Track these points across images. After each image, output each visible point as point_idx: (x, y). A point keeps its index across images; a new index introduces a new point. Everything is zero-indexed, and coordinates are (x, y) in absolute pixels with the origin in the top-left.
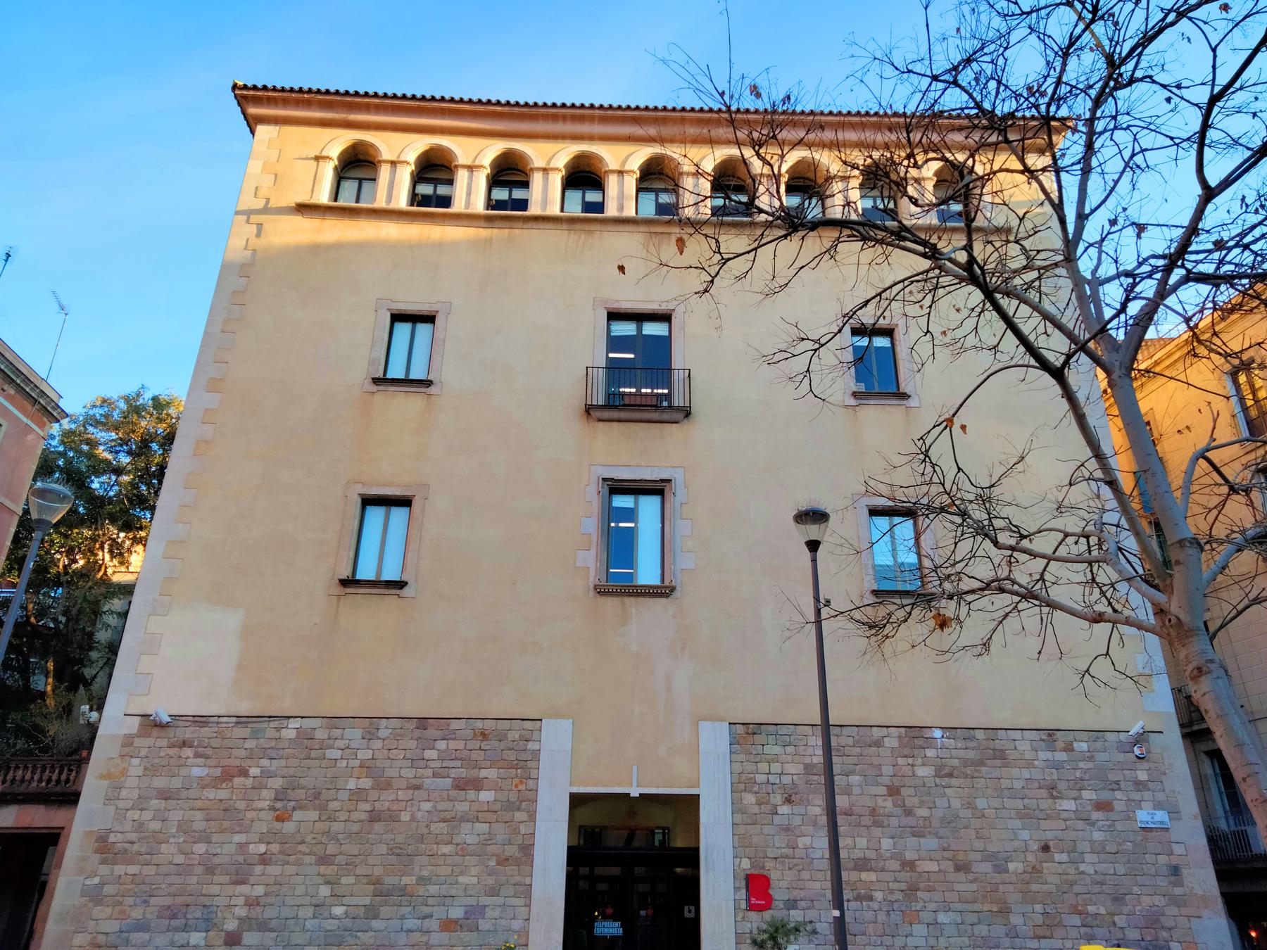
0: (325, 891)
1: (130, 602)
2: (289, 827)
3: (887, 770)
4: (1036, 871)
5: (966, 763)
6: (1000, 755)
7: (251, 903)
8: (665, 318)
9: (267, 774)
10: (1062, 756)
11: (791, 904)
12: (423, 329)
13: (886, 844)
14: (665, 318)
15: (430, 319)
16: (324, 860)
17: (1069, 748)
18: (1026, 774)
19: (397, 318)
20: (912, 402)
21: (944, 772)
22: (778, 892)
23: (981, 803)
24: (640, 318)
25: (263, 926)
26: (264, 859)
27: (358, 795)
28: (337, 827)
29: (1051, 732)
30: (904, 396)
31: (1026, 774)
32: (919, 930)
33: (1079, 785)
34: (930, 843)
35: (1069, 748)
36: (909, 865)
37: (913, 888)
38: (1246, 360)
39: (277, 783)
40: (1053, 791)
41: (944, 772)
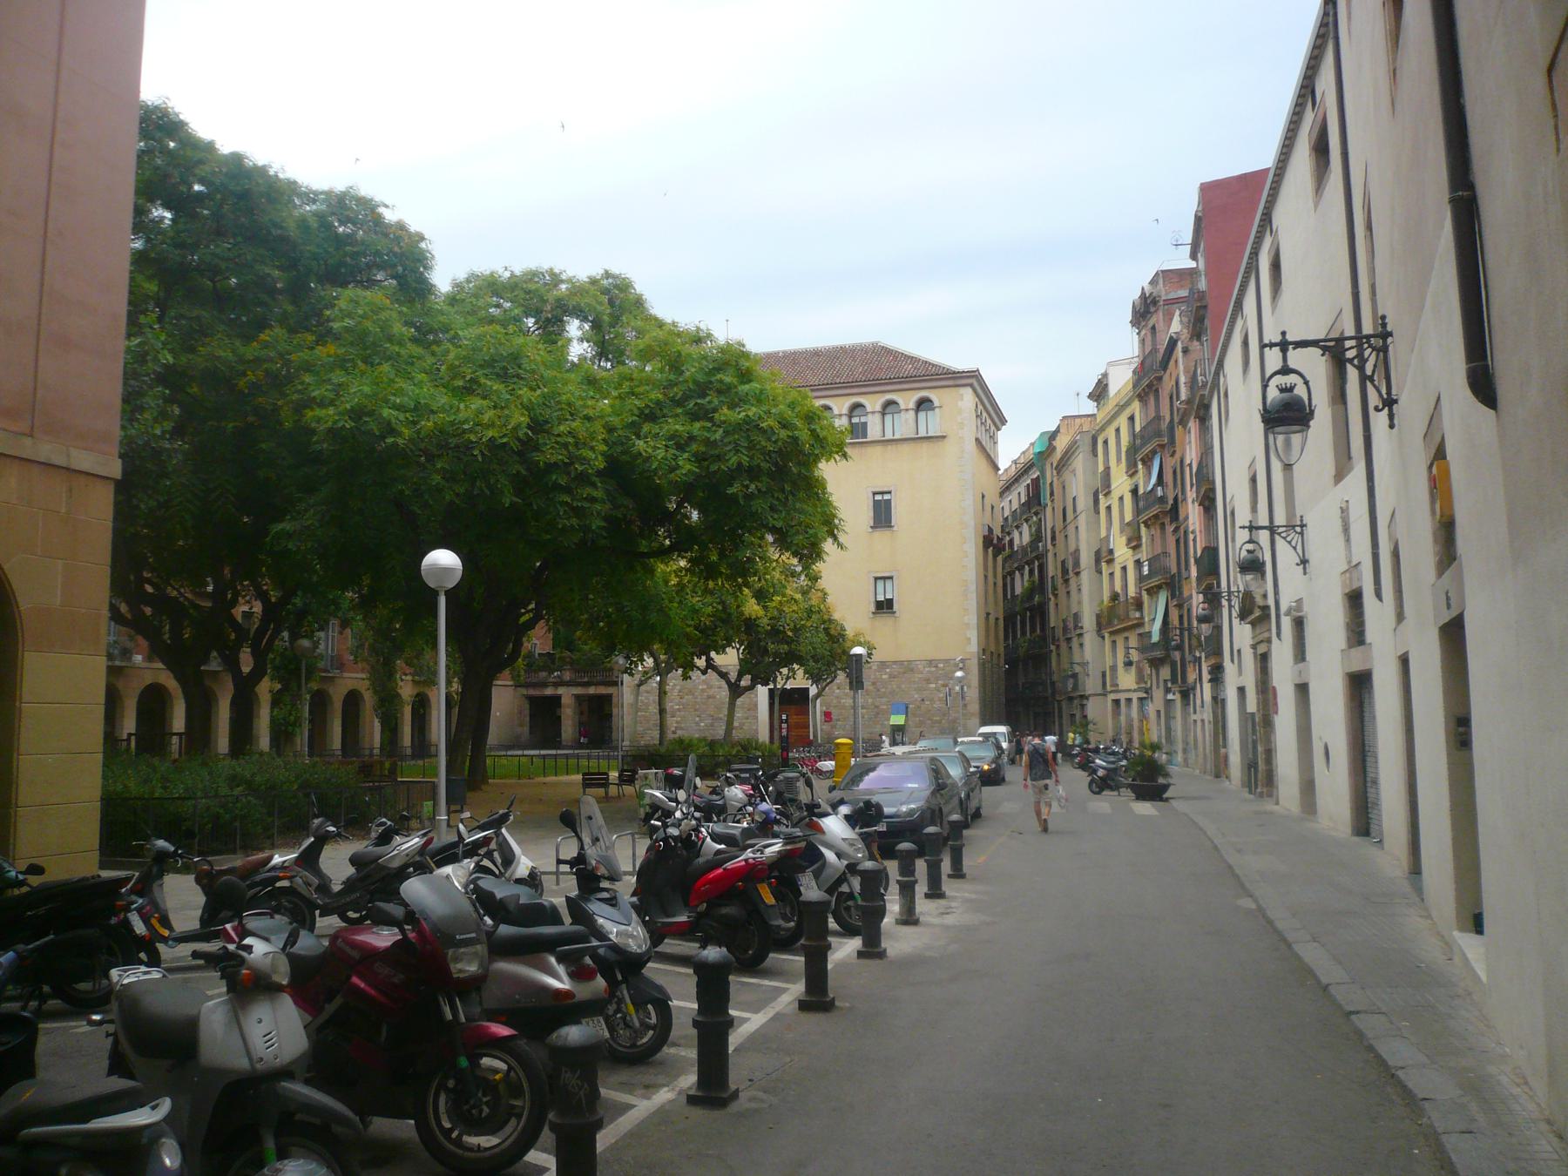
0: (697, 719)
1: (1077, 528)
2: (684, 701)
3: (872, 677)
4: (919, 707)
5: (899, 673)
6: (912, 670)
7: (677, 722)
8: (890, 492)
9: (675, 685)
10: (933, 669)
11: (838, 720)
12: (888, 583)
13: (870, 701)
14: (890, 492)
15: (891, 578)
16: (696, 710)
17: (936, 667)
18: (920, 676)
19: (876, 579)
20: (895, 529)
21: (892, 676)
22: (834, 717)
23: (903, 686)
24: (882, 493)
25: (681, 729)
26: (679, 710)
27: (703, 690)
28: (698, 700)
29: (931, 661)
30: (891, 527)
31: (920, 676)
32: (878, 726)
33: (937, 679)
34: (884, 700)
35: (936, 667)
36: (877, 707)
37: (878, 714)
38: (1375, 328)
39: (678, 687)
40: (928, 681)
41: (892, 676)
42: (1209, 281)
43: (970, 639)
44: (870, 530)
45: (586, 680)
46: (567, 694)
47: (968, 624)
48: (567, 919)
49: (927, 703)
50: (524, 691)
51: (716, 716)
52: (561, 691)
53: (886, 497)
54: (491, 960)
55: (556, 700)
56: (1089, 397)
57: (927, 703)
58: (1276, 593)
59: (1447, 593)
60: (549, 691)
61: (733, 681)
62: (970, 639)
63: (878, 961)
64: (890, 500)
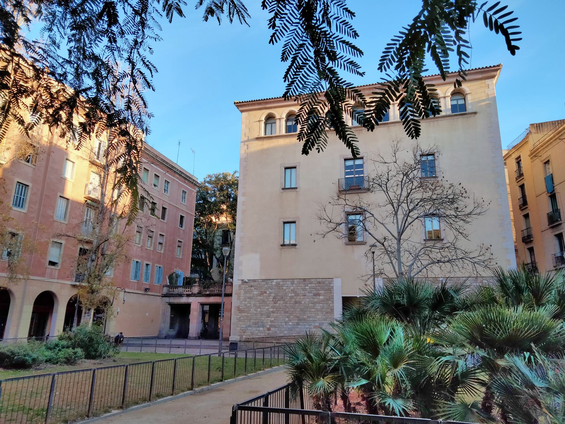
0: (287, 319)
2: (277, 305)
7: (271, 322)
8: (433, 155)
16: (286, 312)
25: (275, 327)
26: (273, 312)
27: (291, 297)
28: (288, 305)
39: (273, 295)
42: (470, 6)
45: (208, 293)
46: (195, 303)
48: (398, 414)
50: (167, 300)
52: (191, 300)
54: (480, 367)
55: (188, 306)
58: (289, 70)
60: (184, 300)
61: (462, 55)
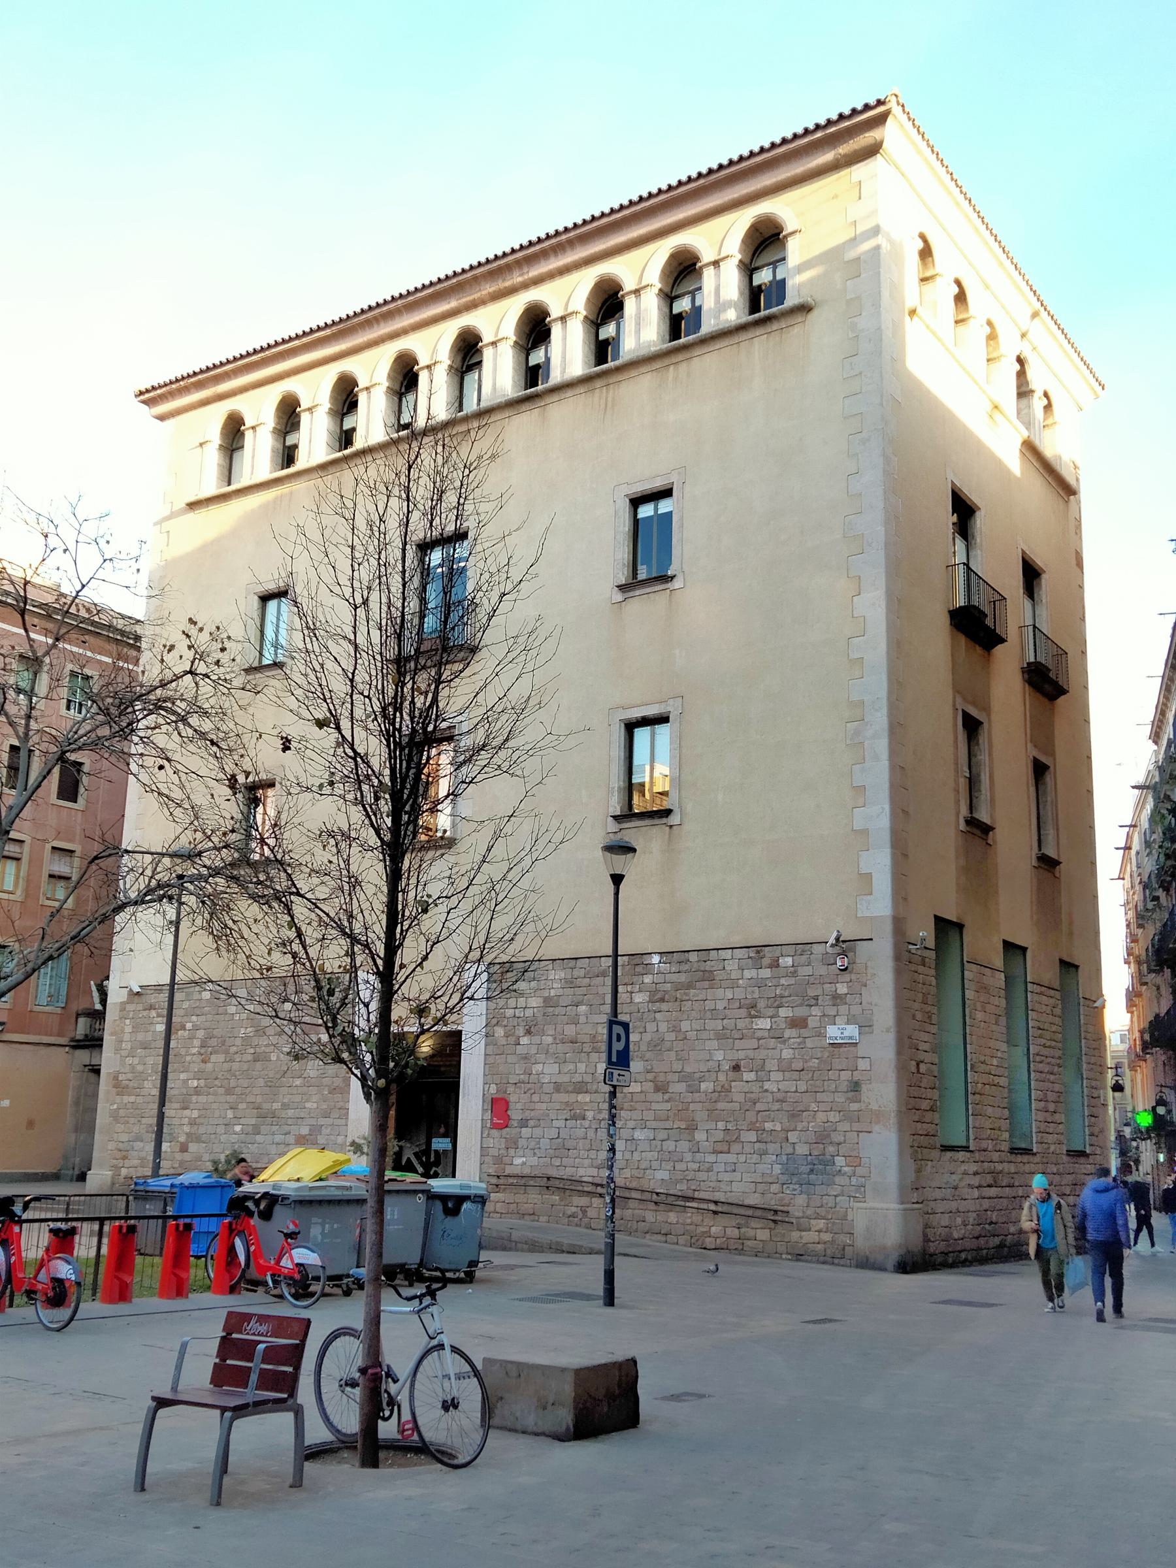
0: (230, 1114)
2: (209, 1066)
5: (678, 987)
7: (192, 1123)
9: (196, 1028)
10: (766, 973)
12: (663, 730)
14: (667, 493)
20: (677, 584)
25: (198, 1139)
26: (197, 1091)
29: (759, 948)
33: (777, 1003)
39: (201, 1034)
43: (869, 876)
44: (619, 597)
47: (865, 832)
49: (747, 1076)
51: (266, 1106)
53: (665, 506)
56: (634, 1362)
57: (747, 1076)
59: (184, 632)
62: (869, 876)
63: (1037, 443)
64: (669, 515)
